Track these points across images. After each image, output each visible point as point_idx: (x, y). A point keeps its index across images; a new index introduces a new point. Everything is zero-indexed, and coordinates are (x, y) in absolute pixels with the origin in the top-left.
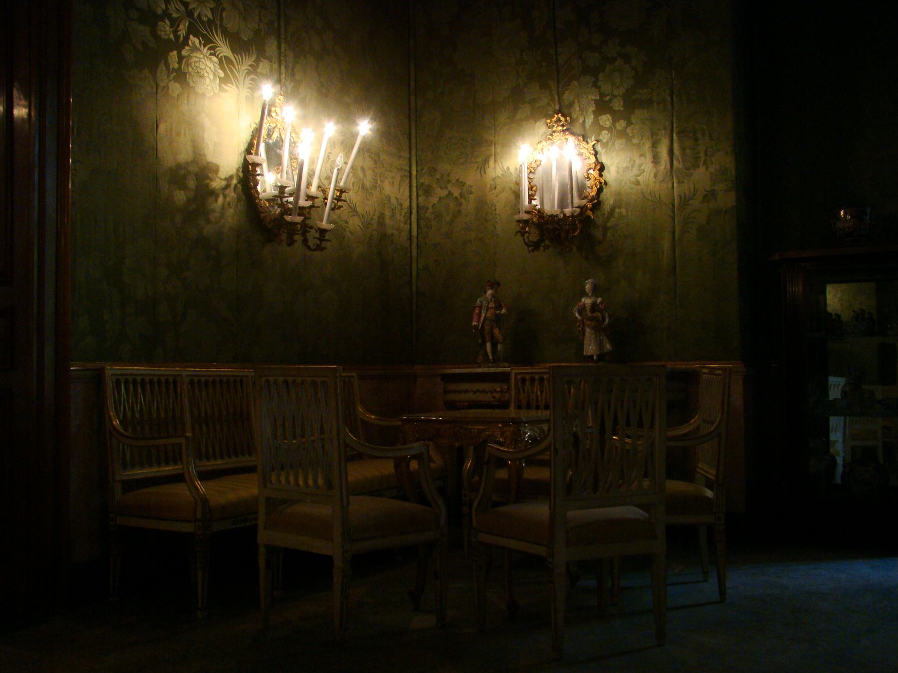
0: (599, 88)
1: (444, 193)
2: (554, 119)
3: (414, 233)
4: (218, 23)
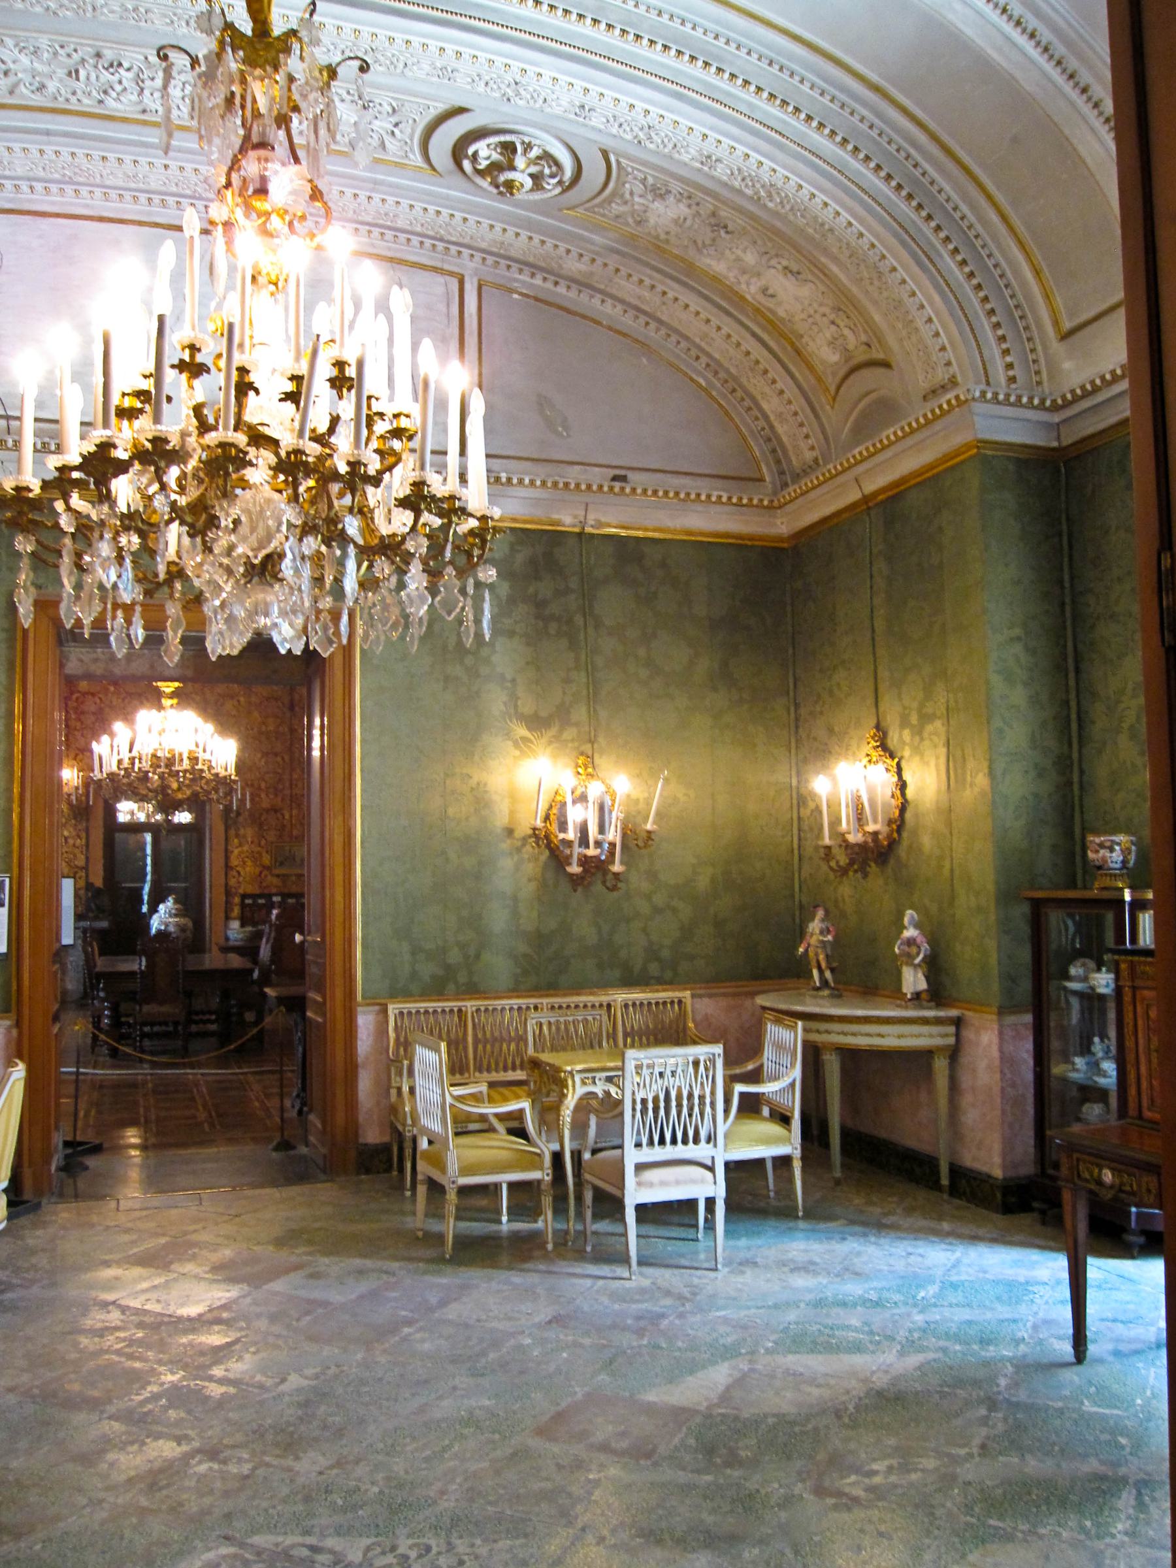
3: (796, 846)
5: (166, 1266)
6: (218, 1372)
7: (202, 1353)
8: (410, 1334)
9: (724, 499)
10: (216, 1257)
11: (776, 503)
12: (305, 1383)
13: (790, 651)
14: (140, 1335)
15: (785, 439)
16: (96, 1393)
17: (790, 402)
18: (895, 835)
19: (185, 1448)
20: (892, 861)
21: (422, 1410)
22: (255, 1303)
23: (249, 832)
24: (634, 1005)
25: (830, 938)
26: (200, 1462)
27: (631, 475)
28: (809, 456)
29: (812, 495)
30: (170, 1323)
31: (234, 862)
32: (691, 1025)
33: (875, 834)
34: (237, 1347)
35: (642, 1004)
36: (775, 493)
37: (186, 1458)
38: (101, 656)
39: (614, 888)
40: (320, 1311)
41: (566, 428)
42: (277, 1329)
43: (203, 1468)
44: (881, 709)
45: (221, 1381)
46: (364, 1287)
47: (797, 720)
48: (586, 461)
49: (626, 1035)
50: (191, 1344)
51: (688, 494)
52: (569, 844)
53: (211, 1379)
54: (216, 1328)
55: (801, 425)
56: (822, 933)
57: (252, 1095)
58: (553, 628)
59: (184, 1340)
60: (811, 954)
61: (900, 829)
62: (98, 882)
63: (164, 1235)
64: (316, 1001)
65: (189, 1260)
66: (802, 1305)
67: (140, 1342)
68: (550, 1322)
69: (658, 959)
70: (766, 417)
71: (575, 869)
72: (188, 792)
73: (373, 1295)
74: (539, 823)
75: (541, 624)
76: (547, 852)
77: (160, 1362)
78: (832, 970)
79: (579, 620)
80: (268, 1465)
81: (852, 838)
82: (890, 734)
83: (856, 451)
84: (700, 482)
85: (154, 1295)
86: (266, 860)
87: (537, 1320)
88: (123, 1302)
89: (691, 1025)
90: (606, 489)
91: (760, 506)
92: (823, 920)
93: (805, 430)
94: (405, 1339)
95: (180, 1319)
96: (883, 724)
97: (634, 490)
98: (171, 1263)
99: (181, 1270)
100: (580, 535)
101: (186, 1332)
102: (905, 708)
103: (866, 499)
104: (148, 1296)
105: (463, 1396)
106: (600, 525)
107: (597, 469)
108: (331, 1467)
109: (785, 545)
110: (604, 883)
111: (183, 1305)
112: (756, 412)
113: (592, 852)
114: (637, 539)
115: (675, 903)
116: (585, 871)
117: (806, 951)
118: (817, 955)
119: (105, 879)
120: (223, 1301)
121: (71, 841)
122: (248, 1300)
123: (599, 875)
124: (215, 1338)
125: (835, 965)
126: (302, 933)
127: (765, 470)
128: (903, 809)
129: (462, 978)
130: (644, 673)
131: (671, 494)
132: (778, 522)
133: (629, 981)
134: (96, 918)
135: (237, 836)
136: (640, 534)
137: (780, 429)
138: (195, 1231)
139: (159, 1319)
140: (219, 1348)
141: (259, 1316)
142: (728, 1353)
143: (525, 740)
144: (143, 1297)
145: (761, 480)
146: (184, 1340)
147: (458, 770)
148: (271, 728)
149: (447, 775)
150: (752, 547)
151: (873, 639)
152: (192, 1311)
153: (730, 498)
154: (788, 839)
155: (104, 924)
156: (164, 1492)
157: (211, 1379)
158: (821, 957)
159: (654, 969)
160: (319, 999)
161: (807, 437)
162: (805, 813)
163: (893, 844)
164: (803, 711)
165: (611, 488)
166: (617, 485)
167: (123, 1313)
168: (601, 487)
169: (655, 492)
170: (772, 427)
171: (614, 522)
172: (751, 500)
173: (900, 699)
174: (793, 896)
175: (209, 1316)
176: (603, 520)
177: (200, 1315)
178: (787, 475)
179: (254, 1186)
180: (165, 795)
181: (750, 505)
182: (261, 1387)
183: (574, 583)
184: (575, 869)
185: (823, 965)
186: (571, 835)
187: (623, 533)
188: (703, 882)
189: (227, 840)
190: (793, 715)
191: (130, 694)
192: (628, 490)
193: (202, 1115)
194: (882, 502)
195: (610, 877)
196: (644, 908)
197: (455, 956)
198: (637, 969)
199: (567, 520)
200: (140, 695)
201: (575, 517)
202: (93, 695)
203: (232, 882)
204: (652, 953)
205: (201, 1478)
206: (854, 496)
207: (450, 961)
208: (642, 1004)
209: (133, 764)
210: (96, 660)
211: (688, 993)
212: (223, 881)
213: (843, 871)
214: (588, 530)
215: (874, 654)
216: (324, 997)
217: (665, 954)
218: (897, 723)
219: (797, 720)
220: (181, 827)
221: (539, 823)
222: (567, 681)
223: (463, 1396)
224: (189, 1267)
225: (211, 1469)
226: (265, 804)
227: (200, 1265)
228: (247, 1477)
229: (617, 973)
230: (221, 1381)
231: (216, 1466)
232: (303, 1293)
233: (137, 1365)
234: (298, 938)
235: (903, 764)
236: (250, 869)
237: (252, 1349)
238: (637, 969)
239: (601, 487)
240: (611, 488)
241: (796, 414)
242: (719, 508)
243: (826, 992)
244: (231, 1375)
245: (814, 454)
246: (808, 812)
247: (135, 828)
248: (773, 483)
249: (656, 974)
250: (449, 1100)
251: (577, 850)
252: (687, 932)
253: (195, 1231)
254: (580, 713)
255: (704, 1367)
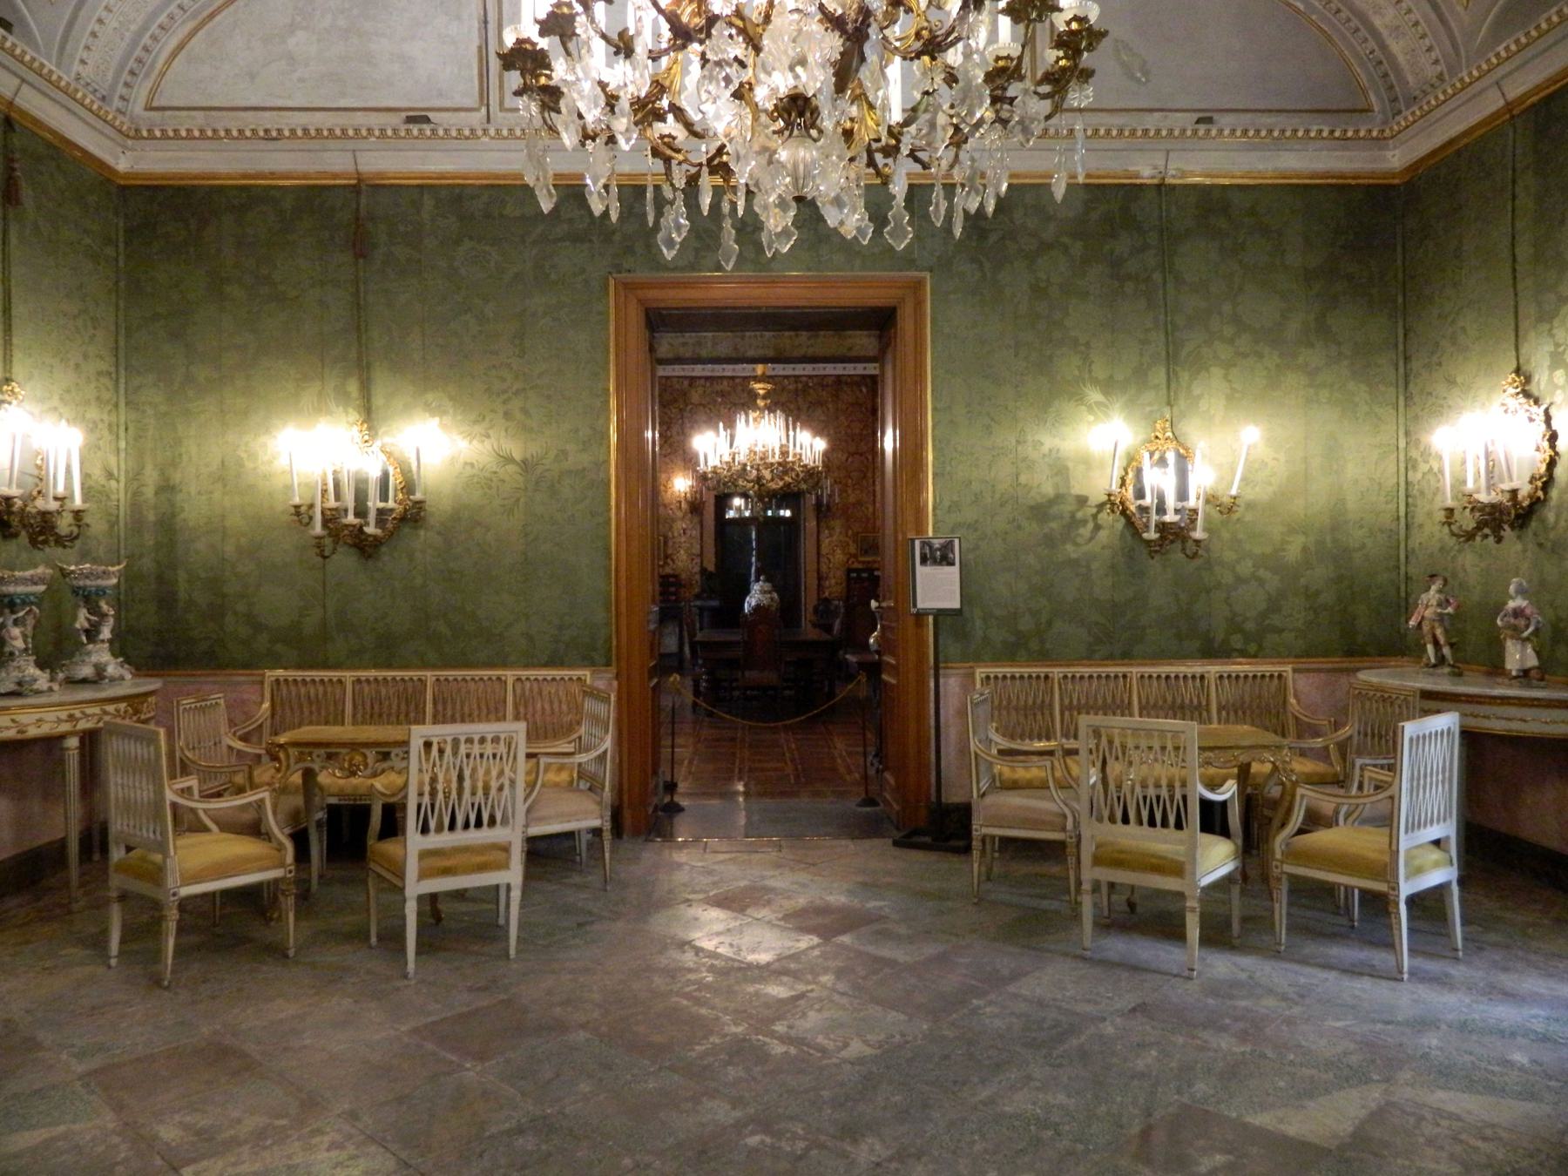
0: (1552, 336)
1: (1427, 467)
2: (1510, 380)
4: (1087, 376)
5: (742, 910)
6: (780, 1028)
7: (767, 1006)
8: (979, 1007)
9: (1325, 134)
10: (789, 905)
11: (1387, 133)
12: (868, 1051)
13: (1400, 300)
14: (710, 979)
15: (1401, 59)
16: (657, 1038)
17: (1409, 11)
18: (1540, 494)
19: (738, 1114)
20: (1534, 524)
21: (990, 1102)
22: (824, 956)
23: (837, 525)
24: (1229, 676)
25: (1450, 610)
26: (753, 1133)
27: (1216, 116)
28: (1431, 72)
29: (1437, 114)
30: (740, 969)
31: (824, 551)
32: (1293, 701)
33: (1514, 492)
34: (802, 1002)
35: (1237, 677)
36: (1385, 122)
37: (739, 1126)
38: (691, 341)
39: (1195, 555)
40: (887, 970)
41: (1146, 73)
42: (841, 987)
43: (754, 1140)
44: (1523, 351)
45: (785, 1039)
46: (930, 950)
47: (1406, 376)
48: (1169, 105)
49: (1220, 708)
50: (757, 994)
51: (1283, 131)
52: (1144, 510)
53: (773, 1034)
54: (785, 979)
55: (1423, 37)
56: (1439, 605)
57: (836, 753)
58: (1129, 287)
59: (751, 989)
60: (1426, 628)
61: (1546, 486)
62: (711, 567)
63: (743, 878)
64: (892, 665)
65: (764, 906)
66: (1444, 1027)
67: (708, 987)
68: (1134, 1010)
69: (1241, 631)
70: (1375, 33)
71: (1152, 535)
72: (781, 483)
73: (942, 959)
74: (1115, 487)
75: (1116, 284)
76: (1123, 520)
77: (725, 1011)
78: (1452, 645)
79: (1157, 276)
80: (822, 1147)
81: (1483, 497)
82: (1536, 378)
83: (1501, 49)
84: (1295, 120)
85: (727, 940)
86: (853, 549)
87: (1118, 1006)
88: (698, 944)
89: (1293, 701)
90: (1189, 133)
91: (1369, 138)
92: (1440, 591)
93: (1427, 42)
94: (974, 1012)
95: (750, 966)
96: (1524, 368)
97: (1221, 131)
98: (747, 907)
99: (756, 915)
100: (1159, 187)
101: (754, 981)
102: (1557, 345)
103: (1509, 106)
104: (722, 939)
105: (1038, 1089)
106: (1184, 174)
107: (1179, 115)
108: (891, 1159)
109: (1396, 181)
110: (1184, 549)
111: (753, 951)
112: (1364, 32)
113: (1170, 517)
114: (1224, 186)
115: (1262, 573)
116: (1162, 538)
117: (1420, 624)
118: (1433, 628)
119: (716, 565)
120: (792, 952)
121: (688, 532)
122: (816, 952)
123: (1178, 545)
124: (777, 990)
125: (1454, 640)
126: (877, 600)
127: (1373, 98)
128: (1552, 464)
129: (1034, 645)
130: (1228, 331)
131: (1263, 133)
132: (1389, 154)
133: (1211, 651)
134: (710, 598)
135: (828, 528)
136: (1227, 182)
137: (1396, 47)
138: (773, 876)
139: (730, 963)
140: (782, 1002)
141: (826, 971)
142: (1353, 1077)
143: (1098, 404)
144: (715, 942)
145: (1369, 110)
146: (751, 989)
147: (1029, 438)
148: (857, 431)
149: (1018, 442)
150: (1358, 185)
151: (1514, 270)
152: (764, 957)
153: (1332, 132)
154: (1392, 506)
155: (715, 603)
156: (713, 1164)
157: (773, 1034)
158: (1439, 632)
159: (1237, 641)
160: (893, 662)
161: (1430, 49)
162: (1414, 477)
163: (1536, 504)
164: (1415, 365)
165: (1195, 132)
166: (1202, 129)
167: (697, 954)
168: (1183, 131)
169: (1245, 132)
170: (1383, 47)
171: (1198, 169)
172: (1357, 132)
173: (1552, 336)
174: (1398, 568)
175: (777, 965)
176: (1185, 168)
177: (768, 964)
178: (1399, 98)
179: (837, 837)
180: (761, 485)
181: (1356, 138)
182: (823, 1050)
183: (1153, 238)
184: (1152, 535)
185: (1442, 640)
186: (1148, 500)
187: (1208, 181)
188: (1293, 552)
189: (818, 532)
190: (1401, 370)
191: (735, 405)
192: (1214, 132)
193: (789, 769)
194: (1533, 105)
195: (1190, 544)
196: (1228, 578)
197: (1026, 624)
198: (1220, 636)
199: (1145, 169)
200: (743, 405)
201: (1155, 168)
202: (704, 406)
203: (824, 568)
204: (1235, 625)
205: (753, 1152)
206: (1492, 103)
207: (1021, 627)
208: (1237, 677)
209: (734, 459)
210: (684, 344)
211: (1289, 668)
212: (815, 567)
213: (1470, 536)
214: (1169, 181)
215: (1515, 286)
216: (897, 661)
217: (1250, 626)
218: (1547, 363)
219: (1406, 376)
220: (784, 518)
221: (1115, 487)
222: (1145, 342)
223: (1038, 1089)
224: (764, 913)
225: (763, 1142)
226: (852, 499)
227: (775, 912)
228: (800, 1158)
229: (1197, 644)
230: (785, 1039)
231: (768, 1140)
232: (871, 949)
233: (703, 1011)
234: (874, 604)
235: (1553, 412)
236: (839, 556)
237: (817, 1007)
238: (1220, 636)
239: (1183, 131)
240: (1195, 132)
241: (1416, 24)
242: (1320, 144)
243: (1447, 670)
244: (793, 1033)
245: (1439, 68)
246: (1419, 475)
247: (741, 522)
248: (1383, 111)
249: (1239, 646)
250: (170, 796)
251: (1154, 517)
252: (1274, 606)
253: (773, 876)
254: (1159, 375)
255: (1327, 1091)
